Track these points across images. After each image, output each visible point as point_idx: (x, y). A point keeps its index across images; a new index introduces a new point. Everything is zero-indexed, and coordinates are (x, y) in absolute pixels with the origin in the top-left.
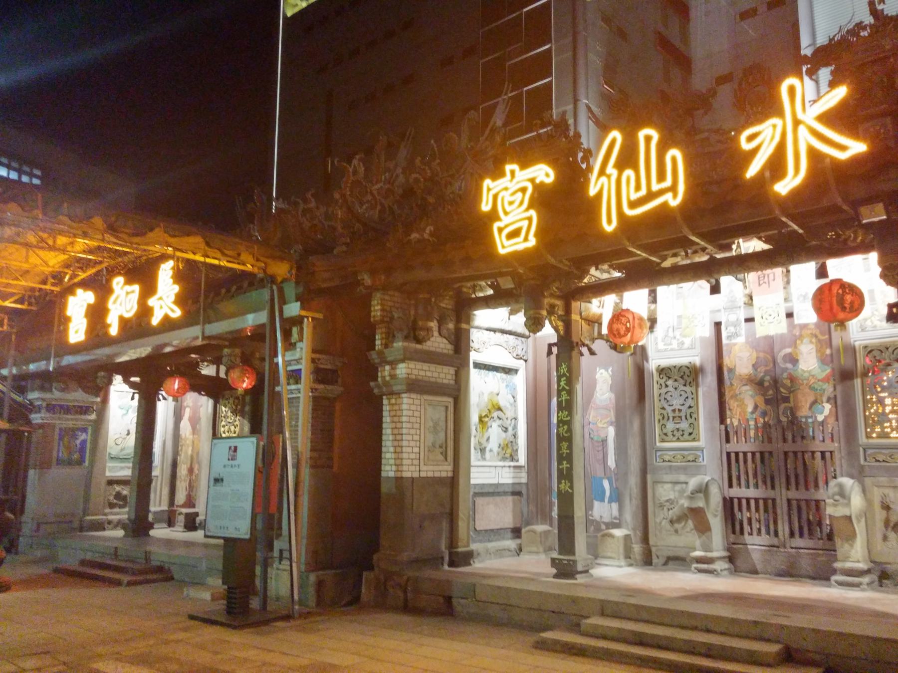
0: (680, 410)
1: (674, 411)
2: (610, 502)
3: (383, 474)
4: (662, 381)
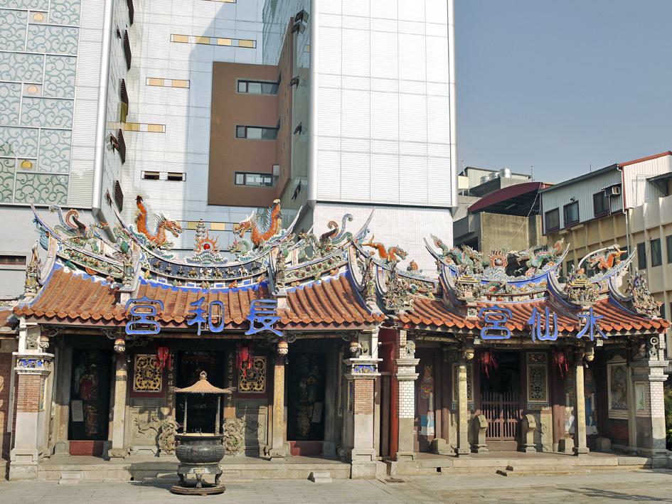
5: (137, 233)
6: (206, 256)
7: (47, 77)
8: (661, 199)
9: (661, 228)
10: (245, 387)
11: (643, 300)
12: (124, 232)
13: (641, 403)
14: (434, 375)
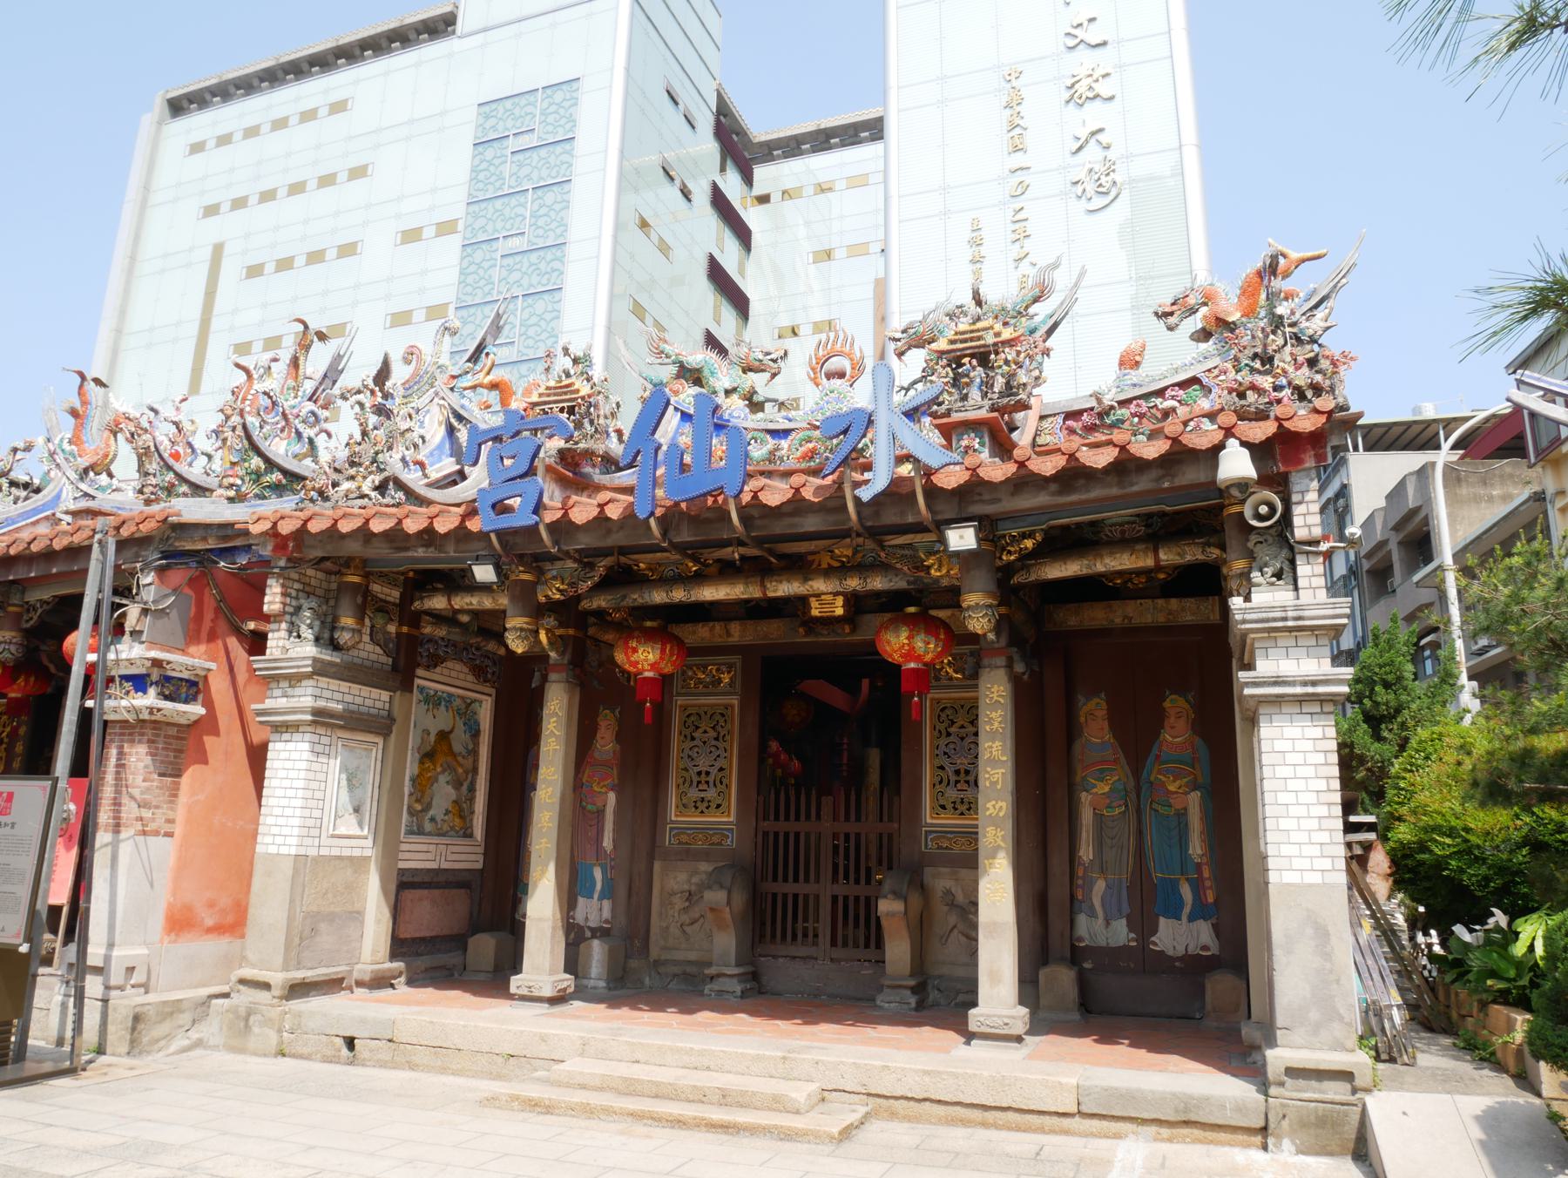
0: (708, 773)
1: (699, 773)
2: (601, 899)
3: (259, 849)
4: (942, 727)
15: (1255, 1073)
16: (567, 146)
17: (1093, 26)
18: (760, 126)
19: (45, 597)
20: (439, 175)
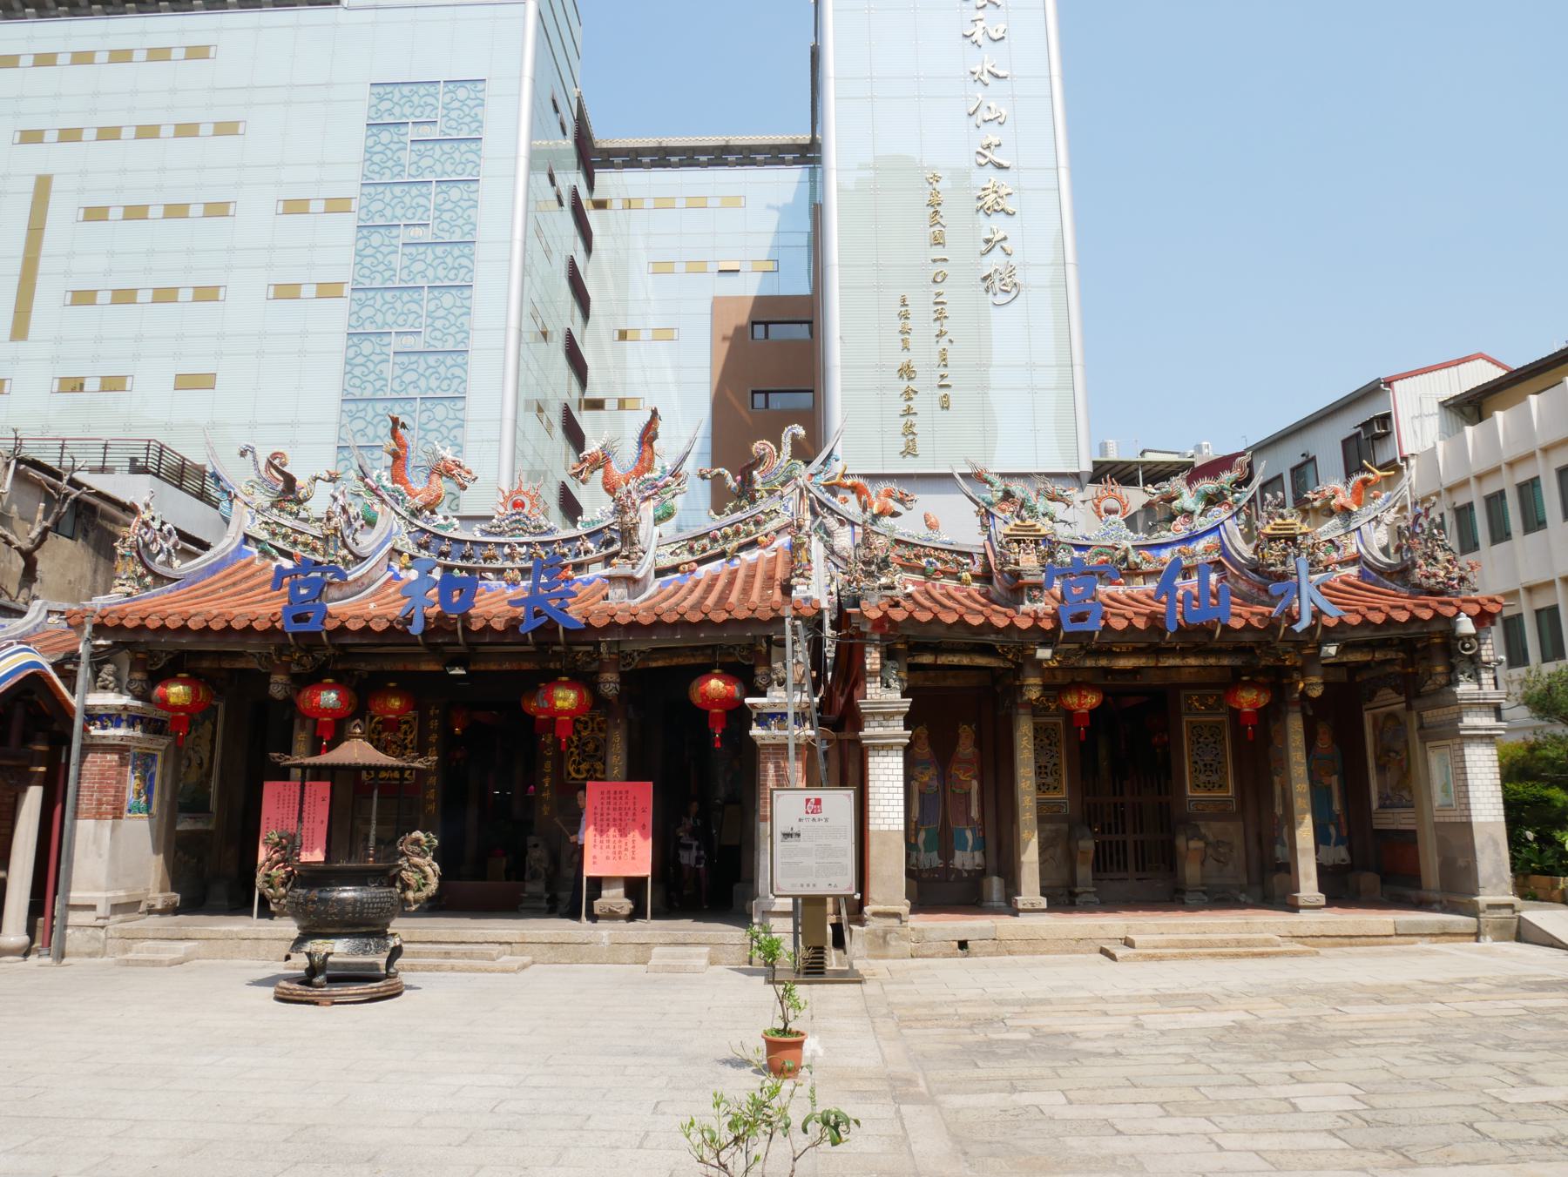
5: (389, 485)
6: (519, 521)
7: (430, 321)
8: (1469, 430)
9: (1472, 481)
10: (578, 771)
11: (1435, 559)
12: (366, 485)
13: (1445, 790)
14: (978, 743)
15: (1472, 910)
16: (473, 146)
17: (997, 150)
18: (604, 136)
19: (643, 648)
20: (335, 153)
